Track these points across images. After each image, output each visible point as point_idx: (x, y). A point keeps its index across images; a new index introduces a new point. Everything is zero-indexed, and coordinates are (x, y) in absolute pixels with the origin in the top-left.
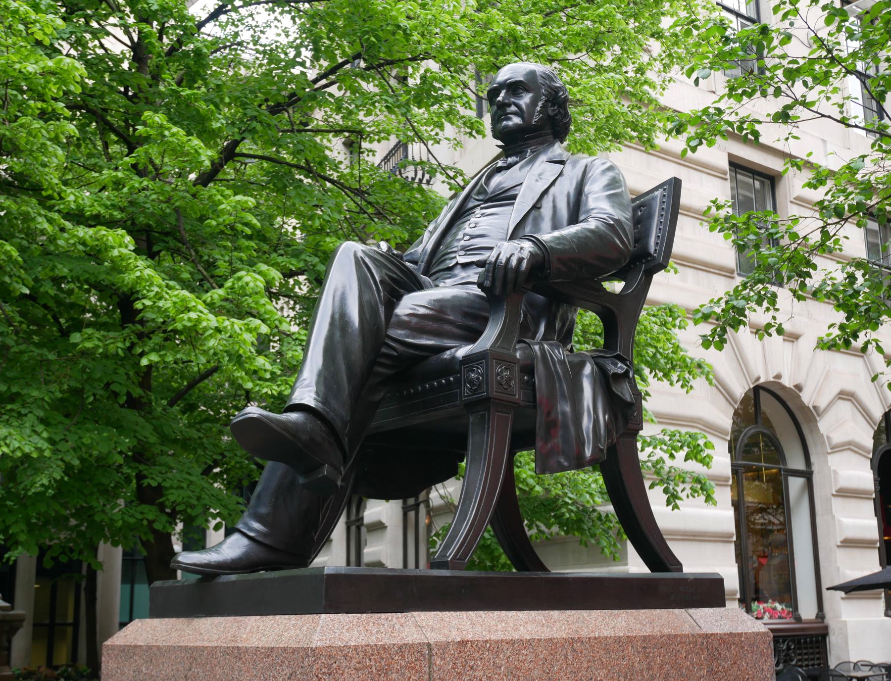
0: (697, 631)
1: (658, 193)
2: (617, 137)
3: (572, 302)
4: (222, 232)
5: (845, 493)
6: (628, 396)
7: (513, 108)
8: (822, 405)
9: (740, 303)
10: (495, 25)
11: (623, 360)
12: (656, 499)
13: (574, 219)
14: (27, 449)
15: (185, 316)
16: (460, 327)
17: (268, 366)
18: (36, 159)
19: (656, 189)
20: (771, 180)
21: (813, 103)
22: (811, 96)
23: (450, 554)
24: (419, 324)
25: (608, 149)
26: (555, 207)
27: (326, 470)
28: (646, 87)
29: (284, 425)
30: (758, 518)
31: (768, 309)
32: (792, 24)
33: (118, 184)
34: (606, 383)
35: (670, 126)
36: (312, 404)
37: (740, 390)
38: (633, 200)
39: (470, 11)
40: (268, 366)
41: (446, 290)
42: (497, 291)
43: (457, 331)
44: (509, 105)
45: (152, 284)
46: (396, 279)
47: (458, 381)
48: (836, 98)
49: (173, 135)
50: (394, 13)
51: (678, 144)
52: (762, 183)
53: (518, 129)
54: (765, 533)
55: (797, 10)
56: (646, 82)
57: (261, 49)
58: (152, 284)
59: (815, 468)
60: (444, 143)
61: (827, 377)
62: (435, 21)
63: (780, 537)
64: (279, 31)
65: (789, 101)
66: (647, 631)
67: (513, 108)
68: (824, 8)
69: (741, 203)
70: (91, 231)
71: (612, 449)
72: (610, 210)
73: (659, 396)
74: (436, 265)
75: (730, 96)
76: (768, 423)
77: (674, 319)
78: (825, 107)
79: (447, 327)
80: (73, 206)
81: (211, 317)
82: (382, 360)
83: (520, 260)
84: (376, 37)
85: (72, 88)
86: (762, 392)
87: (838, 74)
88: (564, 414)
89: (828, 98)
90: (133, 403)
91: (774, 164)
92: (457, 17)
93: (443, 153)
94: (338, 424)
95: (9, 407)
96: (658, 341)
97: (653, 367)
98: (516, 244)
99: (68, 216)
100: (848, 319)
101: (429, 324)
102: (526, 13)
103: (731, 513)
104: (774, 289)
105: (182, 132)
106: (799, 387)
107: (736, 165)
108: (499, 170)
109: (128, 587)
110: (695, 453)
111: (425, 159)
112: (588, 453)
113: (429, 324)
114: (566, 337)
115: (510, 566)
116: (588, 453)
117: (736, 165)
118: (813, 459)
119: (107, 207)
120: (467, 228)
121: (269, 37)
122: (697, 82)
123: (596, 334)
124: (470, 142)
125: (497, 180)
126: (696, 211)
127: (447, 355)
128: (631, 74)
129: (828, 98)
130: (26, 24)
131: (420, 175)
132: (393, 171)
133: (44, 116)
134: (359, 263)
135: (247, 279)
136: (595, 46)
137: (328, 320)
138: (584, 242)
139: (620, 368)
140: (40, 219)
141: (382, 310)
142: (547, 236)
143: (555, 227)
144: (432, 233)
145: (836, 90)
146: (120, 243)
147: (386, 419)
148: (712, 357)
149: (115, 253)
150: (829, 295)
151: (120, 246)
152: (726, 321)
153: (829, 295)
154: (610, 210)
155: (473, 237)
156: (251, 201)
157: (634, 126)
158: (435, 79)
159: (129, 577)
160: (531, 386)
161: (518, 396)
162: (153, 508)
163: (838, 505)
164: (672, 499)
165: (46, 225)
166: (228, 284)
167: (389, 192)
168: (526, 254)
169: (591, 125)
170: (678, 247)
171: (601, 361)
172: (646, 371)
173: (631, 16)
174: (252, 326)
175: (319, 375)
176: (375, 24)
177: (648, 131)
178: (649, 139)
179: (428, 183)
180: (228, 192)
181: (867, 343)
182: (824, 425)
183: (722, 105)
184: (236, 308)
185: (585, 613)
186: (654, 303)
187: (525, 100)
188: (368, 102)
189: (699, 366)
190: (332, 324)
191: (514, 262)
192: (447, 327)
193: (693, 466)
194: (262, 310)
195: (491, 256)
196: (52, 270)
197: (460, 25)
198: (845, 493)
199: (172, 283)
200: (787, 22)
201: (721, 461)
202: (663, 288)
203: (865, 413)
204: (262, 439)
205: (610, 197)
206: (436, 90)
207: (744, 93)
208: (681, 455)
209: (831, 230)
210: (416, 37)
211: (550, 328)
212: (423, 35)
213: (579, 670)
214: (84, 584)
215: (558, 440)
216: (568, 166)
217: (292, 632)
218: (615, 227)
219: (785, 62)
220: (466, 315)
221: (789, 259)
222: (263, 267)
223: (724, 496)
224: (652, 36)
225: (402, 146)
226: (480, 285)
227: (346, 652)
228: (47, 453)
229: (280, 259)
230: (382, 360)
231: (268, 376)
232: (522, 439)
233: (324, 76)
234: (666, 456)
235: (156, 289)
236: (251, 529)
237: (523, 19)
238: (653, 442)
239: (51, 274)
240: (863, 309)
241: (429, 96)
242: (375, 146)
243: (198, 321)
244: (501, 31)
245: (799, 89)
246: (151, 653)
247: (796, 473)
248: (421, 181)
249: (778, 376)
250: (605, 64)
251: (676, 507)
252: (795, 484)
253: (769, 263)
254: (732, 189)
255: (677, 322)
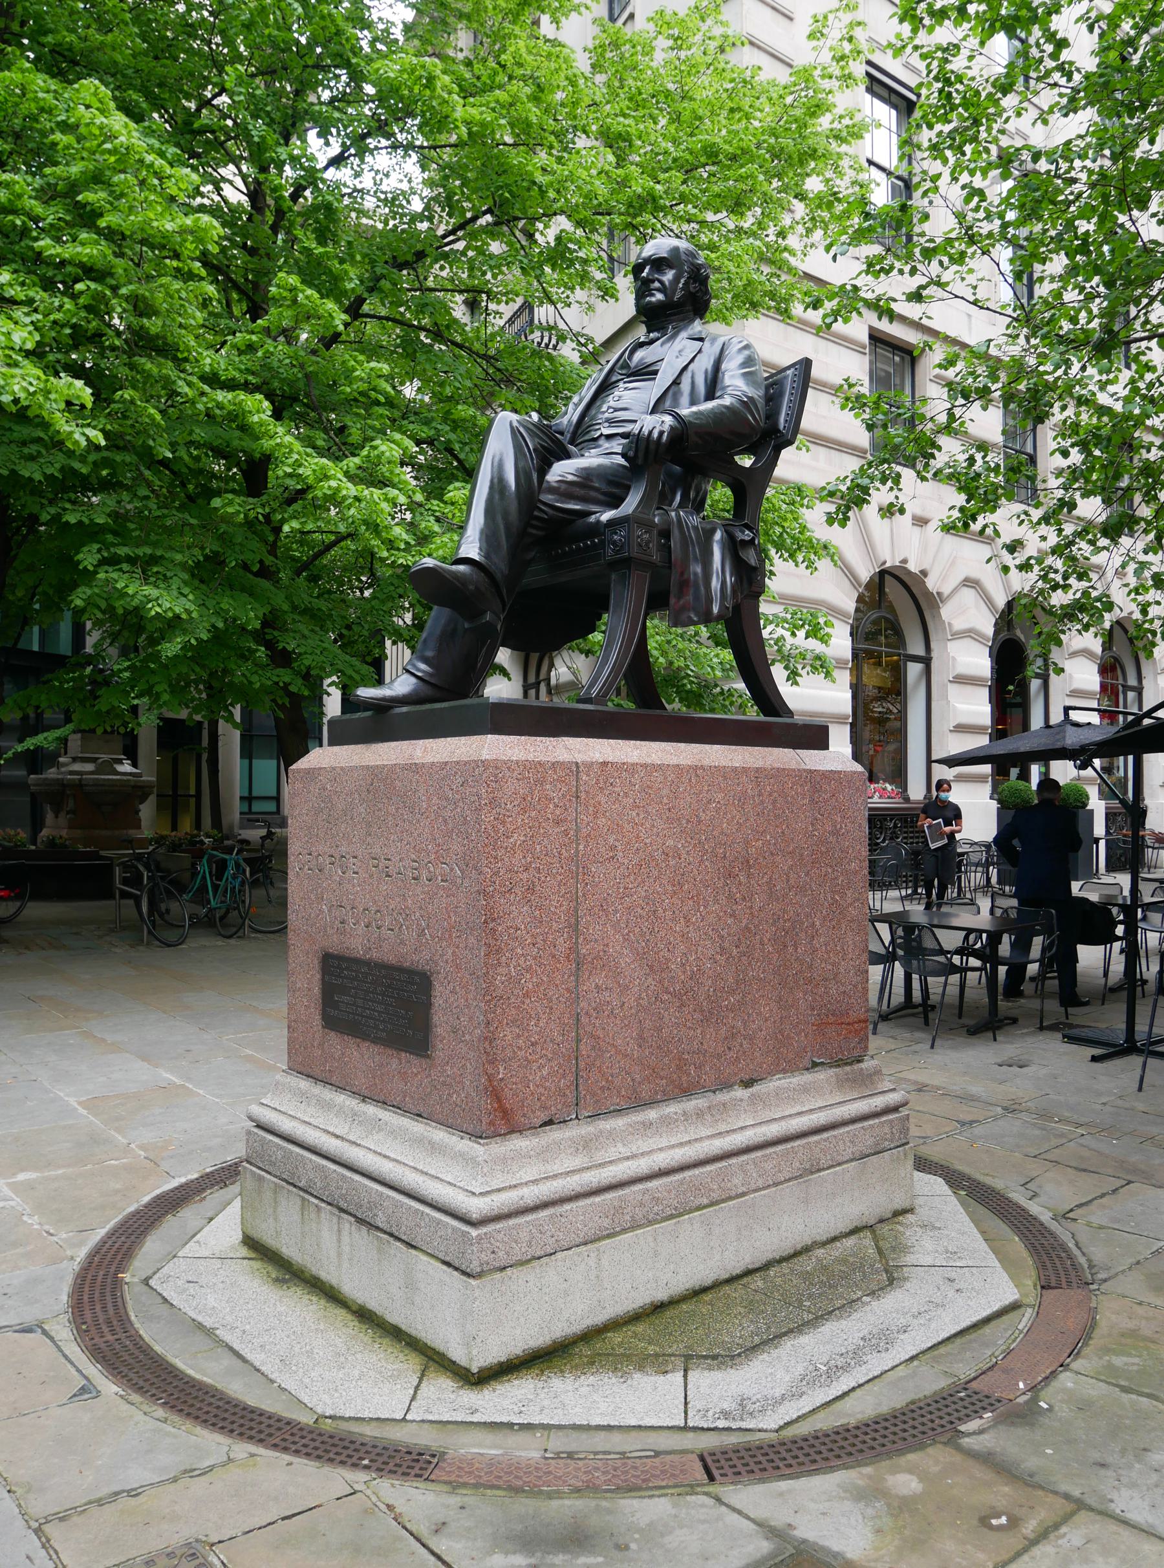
0: (803, 766)
1: (789, 372)
2: (754, 306)
3: (705, 474)
4: (355, 400)
5: (962, 680)
6: (753, 561)
7: (657, 284)
8: (946, 591)
9: (865, 481)
10: (633, 183)
11: (750, 529)
12: (778, 673)
13: (710, 395)
14: (177, 610)
15: (325, 484)
16: (604, 494)
17: (405, 536)
18: (174, 320)
19: (788, 368)
20: (908, 356)
21: (947, 284)
22: (946, 276)
23: (594, 692)
24: (567, 490)
25: (744, 317)
26: (693, 383)
27: (488, 616)
28: (786, 255)
29: (455, 574)
30: (878, 708)
31: (891, 489)
32: (931, 202)
33: (251, 348)
34: (733, 547)
35: (807, 300)
36: (477, 558)
37: (865, 573)
38: (767, 379)
39: (607, 168)
40: (405, 536)
41: (592, 459)
42: (640, 462)
43: (601, 497)
44: (653, 281)
45: (291, 451)
46: (549, 447)
47: (602, 542)
48: (971, 279)
49: (307, 297)
50: (529, 168)
51: (815, 316)
52: (902, 358)
53: (660, 305)
54: (881, 721)
55: (937, 188)
56: (786, 249)
57: (383, 196)
58: (291, 451)
59: (934, 654)
60: (575, 306)
61: (953, 563)
62: (571, 177)
63: (897, 724)
64: (401, 177)
65: (924, 281)
66: (759, 764)
67: (657, 284)
68: (963, 187)
69: (878, 379)
70: (230, 396)
71: (737, 608)
72: (745, 388)
73: (785, 578)
74: (583, 434)
75: (867, 272)
76: (891, 609)
77: (803, 498)
78: (959, 288)
79: (593, 494)
80: (207, 369)
81: (350, 485)
82: (534, 522)
83: (661, 433)
84: (510, 192)
85: (210, 247)
86: (887, 577)
87: (974, 253)
88: (696, 574)
89: (963, 279)
90: (265, 572)
91: (911, 337)
92: (594, 172)
93: (573, 318)
94: (499, 576)
95: (155, 569)
96: (785, 520)
97: (779, 547)
98: (657, 417)
99: (203, 378)
100: (968, 501)
101: (578, 491)
102: (666, 171)
103: (848, 695)
104: (899, 468)
105: (316, 295)
106: (924, 573)
107: (877, 339)
108: (642, 345)
109: (247, 761)
110: (815, 632)
111: (552, 323)
112: (715, 610)
113: (578, 491)
114: (699, 506)
115: (645, 703)
116: (715, 610)
117: (877, 339)
118: (933, 645)
119: (241, 371)
120: (611, 401)
121: (390, 184)
122: (834, 258)
123: (724, 510)
124: (600, 305)
125: (639, 355)
126: (831, 387)
127: (592, 519)
128: (772, 238)
129: (963, 279)
130: (160, 179)
131: (546, 340)
132: (518, 334)
133: (179, 274)
134: (514, 432)
135: (383, 448)
136: (737, 206)
137: (487, 484)
138: (719, 417)
139: (747, 535)
140: (181, 383)
141: (535, 476)
142: (685, 411)
143: (693, 402)
144: (577, 405)
145: (971, 271)
146: (258, 408)
147: (536, 576)
148: (837, 536)
149: (256, 418)
150: (950, 477)
151: (258, 412)
152: (851, 499)
153: (950, 477)
154: (745, 388)
155: (616, 410)
156: (385, 368)
157: (772, 295)
158: (571, 241)
159: (248, 752)
160: (667, 548)
161: (656, 557)
162: (289, 671)
163: (954, 690)
164: (793, 677)
165: (187, 389)
166: (365, 452)
167: (518, 359)
168: (666, 428)
169: (728, 291)
170: (808, 422)
171: (730, 529)
172: (773, 552)
173: (775, 176)
174: (390, 496)
175: (482, 532)
176: (510, 180)
177: (786, 301)
178: (786, 310)
179: (555, 348)
180: (361, 358)
181: (985, 526)
182: (946, 612)
183: (858, 283)
184: (371, 477)
185: (707, 747)
186: (782, 481)
187: (668, 276)
188: (497, 263)
189: (825, 547)
190: (491, 487)
191: (655, 435)
192: (593, 494)
193: (814, 645)
194: (396, 480)
195: (635, 428)
196: (190, 434)
197: (597, 183)
198: (962, 680)
199: (309, 450)
200: (926, 200)
201: (841, 643)
202: (793, 465)
203: (988, 600)
204: (433, 586)
205: (744, 374)
206: (571, 251)
207: (882, 269)
208: (801, 634)
209: (957, 412)
210: (552, 194)
211: (685, 497)
212: (558, 192)
213: (701, 792)
214: (205, 756)
215: (690, 598)
216: (707, 343)
217: (463, 750)
218: (748, 404)
219: (922, 240)
220: (611, 483)
221: (916, 440)
222: (397, 436)
223: (844, 678)
224: (796, 197)
225: (527, 307)
226: (624, 455)
227: (509, 765)
228: (195, 615)
229: (411, 427)
230: (534, 522)
231: (402, 546)
232: (657, 601)
233: (453, 232)
234: (787, 634)
235: (296, 456)
236: (419, 670)
237: (662, 176)
238: (777, 620)
239: (189, 439)
240: (981, 491)
241: (563, 257)
242: (502, 308)
243: (338, 489)
244: (640, 190)
245: (934, 268)
246: (337, 774)
247: (916, 659)
248: (547, 346)
249: (905, 561)
250: (746, 225)
251: (796, 683)
252: (914, 670)
253: (901, 443)
254: (871, 362)
255: (805, 502)
